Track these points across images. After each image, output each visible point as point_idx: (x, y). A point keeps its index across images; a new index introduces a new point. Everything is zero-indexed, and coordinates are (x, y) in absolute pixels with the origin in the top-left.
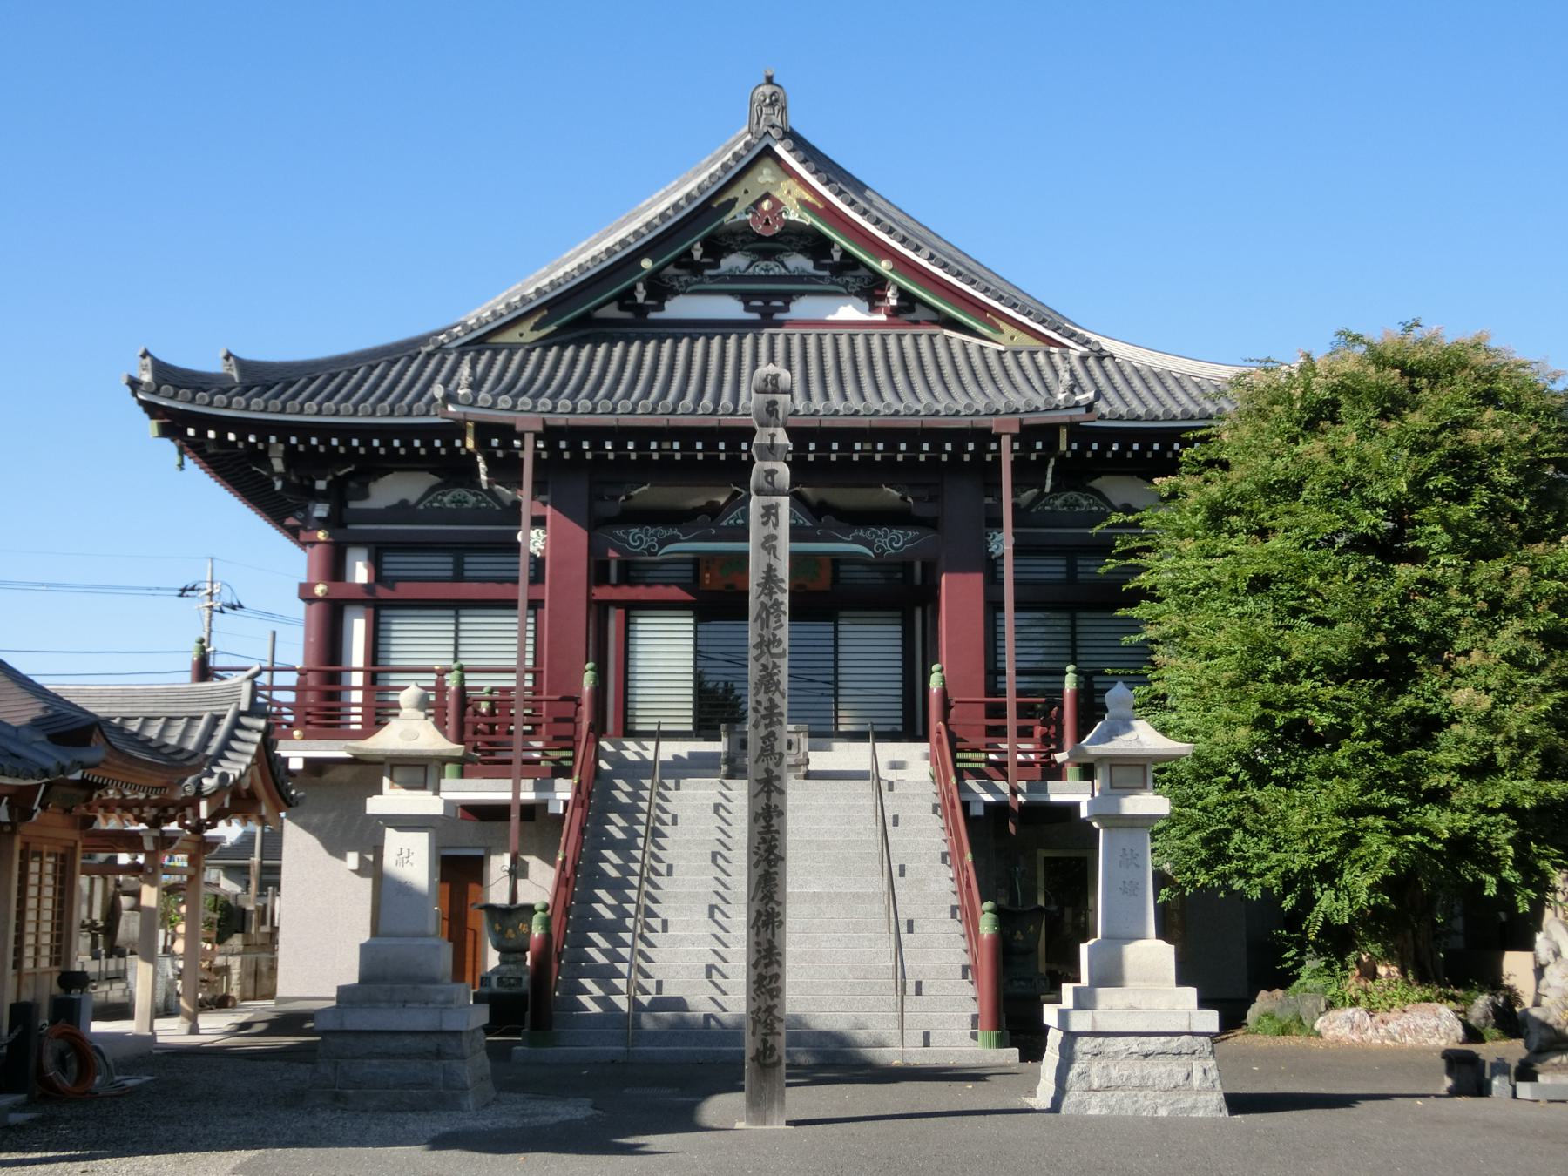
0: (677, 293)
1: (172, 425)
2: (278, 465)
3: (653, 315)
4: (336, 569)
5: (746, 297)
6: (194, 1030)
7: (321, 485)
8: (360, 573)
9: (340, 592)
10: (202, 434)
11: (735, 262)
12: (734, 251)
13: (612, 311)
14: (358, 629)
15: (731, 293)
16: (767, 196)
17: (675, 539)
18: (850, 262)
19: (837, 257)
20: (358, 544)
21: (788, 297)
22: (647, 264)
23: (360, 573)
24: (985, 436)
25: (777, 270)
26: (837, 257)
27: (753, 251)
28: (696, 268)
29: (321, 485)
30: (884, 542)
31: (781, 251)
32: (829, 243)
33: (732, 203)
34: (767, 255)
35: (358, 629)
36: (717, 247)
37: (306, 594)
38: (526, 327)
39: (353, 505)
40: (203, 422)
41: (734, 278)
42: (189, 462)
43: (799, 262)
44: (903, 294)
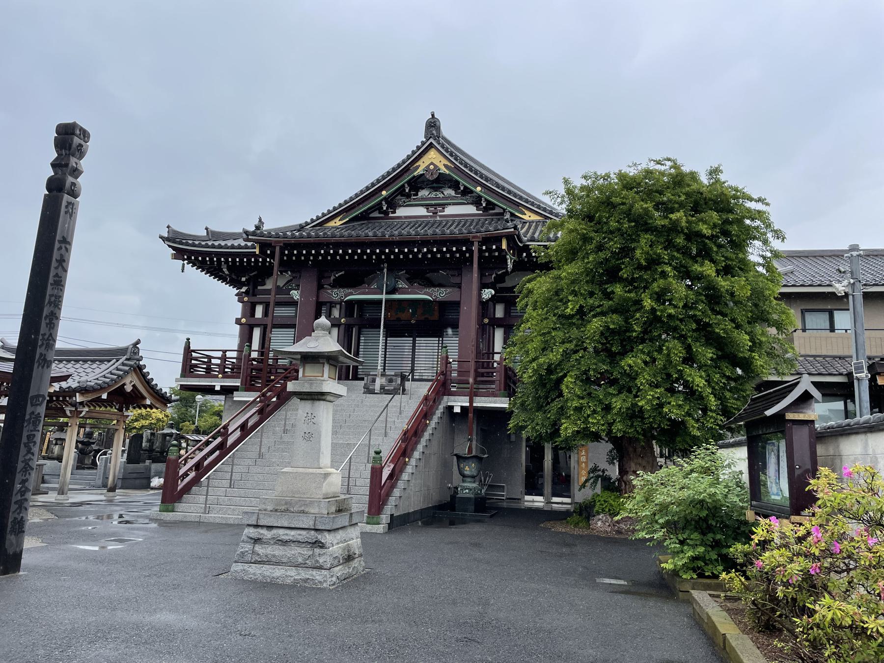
0: (400, 206)
1: (180, 254)
2: (227, 272)
3: (391, 215)
4: (249, 310)
5: (427, 206)
6: (549, 502)
7: (243, 279)
8: (259, 312)
9: (252, 322)
10: (196, 259)
11: (423, 193)
12: (423, 189)
13: (376, 214)
14: (257, 333)
15: (422, 205)
16: (432, 163)
17: (351, 294)
18: (467, 192)
19: (462, 188)
20: (260, 303)
21: (444, 206)
22: (384, 193)
23: (259, 312)
24: (468, 242)
25: (441, 196)
26: (462, 188)
27: (431, 188)
28: (408, 196)
29: (243, 279)
30: (437, 294)
31: (441, 187)
32: (458, 183)
33: (418, 167)
34: (436, 189)
35: (257, 333)
36: (417, 184)
37: (238, 321)
38: (337, 220)
39: (259, 288)
40: (192, 252)
41: (423, 199)
42: (188, 267)
43: (450, 192)
44: (489, 203)
